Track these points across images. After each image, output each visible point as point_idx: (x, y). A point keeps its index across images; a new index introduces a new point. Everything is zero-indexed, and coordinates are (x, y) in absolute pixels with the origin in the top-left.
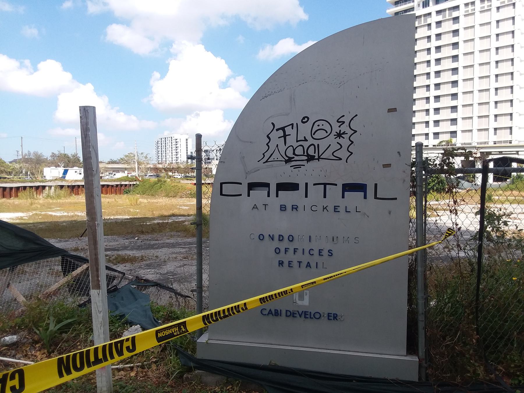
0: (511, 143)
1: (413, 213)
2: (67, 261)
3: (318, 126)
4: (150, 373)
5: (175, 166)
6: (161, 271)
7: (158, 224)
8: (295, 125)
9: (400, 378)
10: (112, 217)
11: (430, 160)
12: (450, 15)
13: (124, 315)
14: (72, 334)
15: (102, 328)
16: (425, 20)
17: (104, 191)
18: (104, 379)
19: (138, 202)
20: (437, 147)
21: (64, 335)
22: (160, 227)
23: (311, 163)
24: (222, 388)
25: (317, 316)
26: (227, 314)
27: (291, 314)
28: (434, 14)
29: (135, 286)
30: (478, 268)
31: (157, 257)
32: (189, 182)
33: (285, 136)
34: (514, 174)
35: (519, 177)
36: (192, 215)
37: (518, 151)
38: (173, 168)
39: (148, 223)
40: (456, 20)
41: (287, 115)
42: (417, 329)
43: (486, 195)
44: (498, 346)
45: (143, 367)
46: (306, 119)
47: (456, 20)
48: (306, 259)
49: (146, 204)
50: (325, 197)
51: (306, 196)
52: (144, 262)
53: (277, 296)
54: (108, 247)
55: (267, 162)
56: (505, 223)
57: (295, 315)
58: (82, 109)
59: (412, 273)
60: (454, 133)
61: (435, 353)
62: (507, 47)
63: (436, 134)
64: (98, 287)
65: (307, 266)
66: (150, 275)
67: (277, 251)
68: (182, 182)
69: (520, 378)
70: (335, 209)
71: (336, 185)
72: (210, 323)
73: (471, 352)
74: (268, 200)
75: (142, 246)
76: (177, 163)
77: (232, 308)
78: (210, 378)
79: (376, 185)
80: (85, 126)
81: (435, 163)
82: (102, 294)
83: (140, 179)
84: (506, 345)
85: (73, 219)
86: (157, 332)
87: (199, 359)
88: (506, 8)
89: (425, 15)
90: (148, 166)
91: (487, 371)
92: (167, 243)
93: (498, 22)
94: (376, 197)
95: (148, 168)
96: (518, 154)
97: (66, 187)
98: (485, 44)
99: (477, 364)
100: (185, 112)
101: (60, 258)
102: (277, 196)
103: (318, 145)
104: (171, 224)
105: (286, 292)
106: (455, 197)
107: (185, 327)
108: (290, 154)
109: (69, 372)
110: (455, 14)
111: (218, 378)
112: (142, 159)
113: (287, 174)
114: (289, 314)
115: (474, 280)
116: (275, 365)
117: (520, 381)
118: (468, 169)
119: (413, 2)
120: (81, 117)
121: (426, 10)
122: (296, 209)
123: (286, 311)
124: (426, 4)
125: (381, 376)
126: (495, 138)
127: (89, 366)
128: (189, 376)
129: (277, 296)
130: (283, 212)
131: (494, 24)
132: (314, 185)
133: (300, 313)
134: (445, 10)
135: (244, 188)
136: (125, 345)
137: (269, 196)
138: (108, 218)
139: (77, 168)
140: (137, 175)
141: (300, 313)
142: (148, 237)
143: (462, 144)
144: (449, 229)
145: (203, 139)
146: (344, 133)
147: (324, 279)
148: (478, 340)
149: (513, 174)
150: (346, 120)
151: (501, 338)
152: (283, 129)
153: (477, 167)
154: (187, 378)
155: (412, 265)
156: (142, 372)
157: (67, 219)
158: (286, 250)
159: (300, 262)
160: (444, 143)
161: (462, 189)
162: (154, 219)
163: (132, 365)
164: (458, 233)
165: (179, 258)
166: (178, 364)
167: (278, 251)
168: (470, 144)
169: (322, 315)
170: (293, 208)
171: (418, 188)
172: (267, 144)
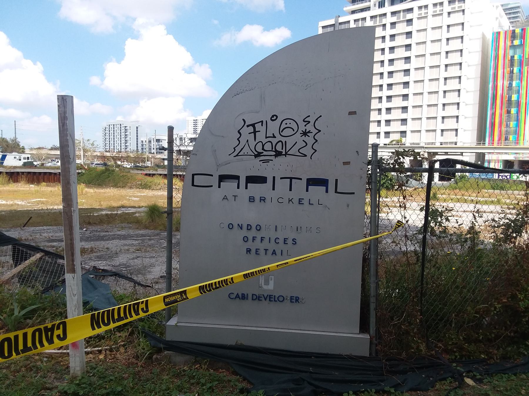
0: (456, 144)
1: (368, 209)
2: (19, 250)
3: (286, 124)
4: (118, 355)
5: (124, 155)
6: (113, 263)
7: (107, 215)
8: (264, 123)
9: (353, 354)
10: (56, 207)
11: (384, 159)
12: (404, 16)
13: (88, 302)
14: (37, 319)
15: (76, 310)
16: (381, 21)
17: (46, 179)
18: (78, 359)
19: (84, 191)
20: (388, 146)
21: (28, 321)
22: (109, 218)
23: (279, 158)
24: (191, 367)
25: (281, 299)
26: (218, 286)
27: (257, 298)
28: (389, 15)
29: (92, 276)
30: (422, 258)
31: (107, 248)
32: (140, 172)
33: (255, 132)
34: (458, 174)
35: (462, 177)
36: (143, 207)
37: (462, 153)
38: (122, 157)
39: (95, 214)
40: (410, 22)
41: (257, 112)
42: (369, 310)
43: (431, 192)
44: (437, 327)
45: (111, 350)
46: (275, 117)
47: (410, 22)
48: (272, 247)
49: (93, 194)
50: (291, 190)
51: (274, 189)
52: (95, 254)
53: (257, 273)
54: (54, 238)
55: (237, 155)
56: (447, 220)
57: (261, 299)
58: (60, 98)
59: (365, 260)
60: (403, 133)
61: (384, 331)
62: (457, 38)
63: (387, 134)
64: (73, 271)
65: (273, 253)
66: (102, 265)
67: (245, 239)
68: (132, 171)
69: (457, 354)
70: (299, 201)
71: (301, 179)
72: (205, 292)
73: (415, 330)
74: (238, 192)
75: (91, 237)
76: (126, 152)
77: (222, 281)
78: (179, 358)
79: (337, 180)
80: (63, 115)
81: (388, 162)
82: (77, 278)
83: (86, 168)
84: (445, 326)
85: (13, 208)
86: (165, 297)
87: (168, 341)
88: (456, 14)
89: (381, 15)
90: (95, 154)
91: (428, 347)
92: (118, 235)
93: (449, 26)
94: (336, 192)
95: (95, 156)
96: (462, 155)
97: (4, 173)
98: (434, 86)
99: (420, 341)
100: (133, 98)
101: (10, 247)
102: (246, 188)
103: (286, 142)
104: (121, 215)
105: (264, 270)
106: (404, 192)
107: (186, 294)
108: (259, 149)
109: (99, 327)
110: (409, 16)
111: (187, 357)
112: (88, 146)
113: (256, 168)
114: (255, 297)
115: (418, 268)
116: (241, 345)
117: (456, 357)
118: (416, 168)
119: (370, 1)
120: (59, 106)
121: (382, 11)
122: (264, 200)
123: (253, 295)
124: (381, 5)
125: (337, 353)
126: (442, 139)
127: (114, 322)
128: (159, 357)
129: (257, 273)
130: (252, 204)
131: (445, 28)
132: (281, 178)
133: (266, 297)
134: (399, 12)
135: (215, 181)
136: (141, 306)
137: (238, 188)
138: (51, 207)
139: (16, 154)
140: (83, 163)
141: (266, 297)
142: (98, 228)
143: (411, 144)
144: (399, 221)
145: (175, 132)
146: (309, 132)
147: (295, 261)
148: (421, 321)
149: (457, 174)
150: (312, 120)
151: (441, 320)
152: (253, 125)
153: (424, 167)
154: (157, 358)
155: (365, 254)
156: (111, 355)
157: (5, 209)
158: (254, 239)
159: (266, 250)
160: (394, 143)
161: (410, 187)
162: (102, 210)
163: (100, 348)
164: (406, 225)
165: (131, 250)
166: (147, 346)
167: (246, 240)
168: (419, 144)
169: (285, 298)
170: (261, 200)
171: (373, 184)
172: (238, 139)
